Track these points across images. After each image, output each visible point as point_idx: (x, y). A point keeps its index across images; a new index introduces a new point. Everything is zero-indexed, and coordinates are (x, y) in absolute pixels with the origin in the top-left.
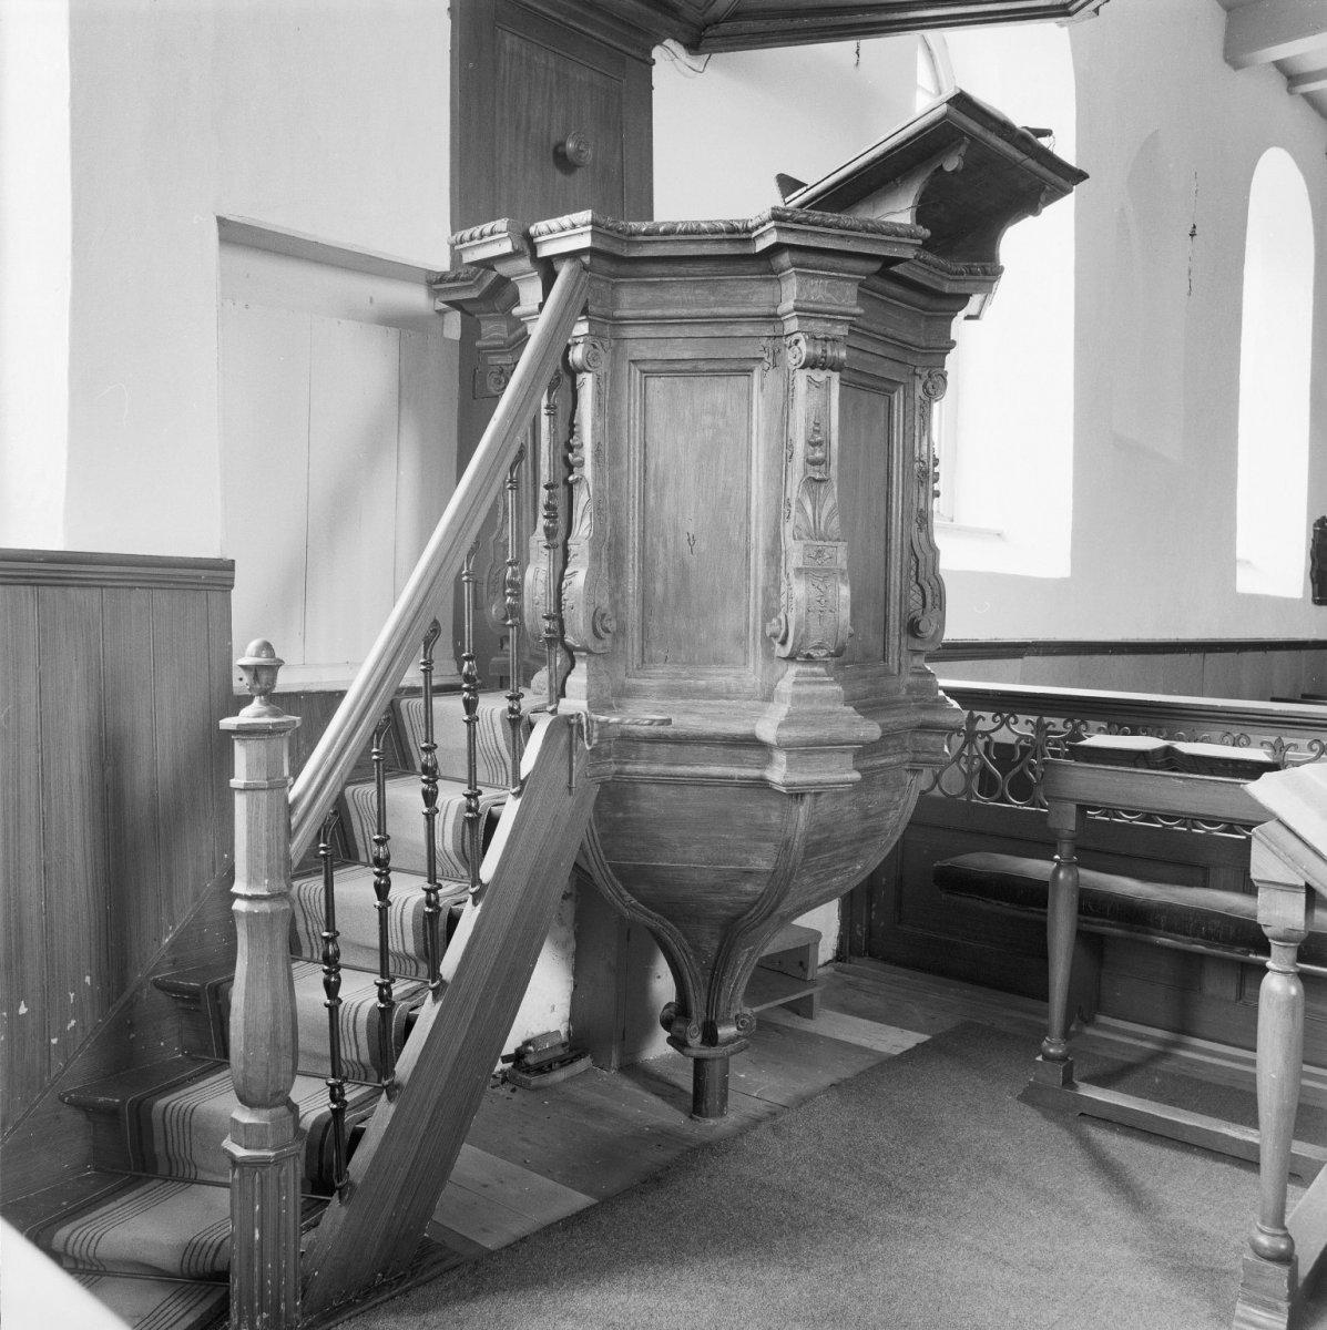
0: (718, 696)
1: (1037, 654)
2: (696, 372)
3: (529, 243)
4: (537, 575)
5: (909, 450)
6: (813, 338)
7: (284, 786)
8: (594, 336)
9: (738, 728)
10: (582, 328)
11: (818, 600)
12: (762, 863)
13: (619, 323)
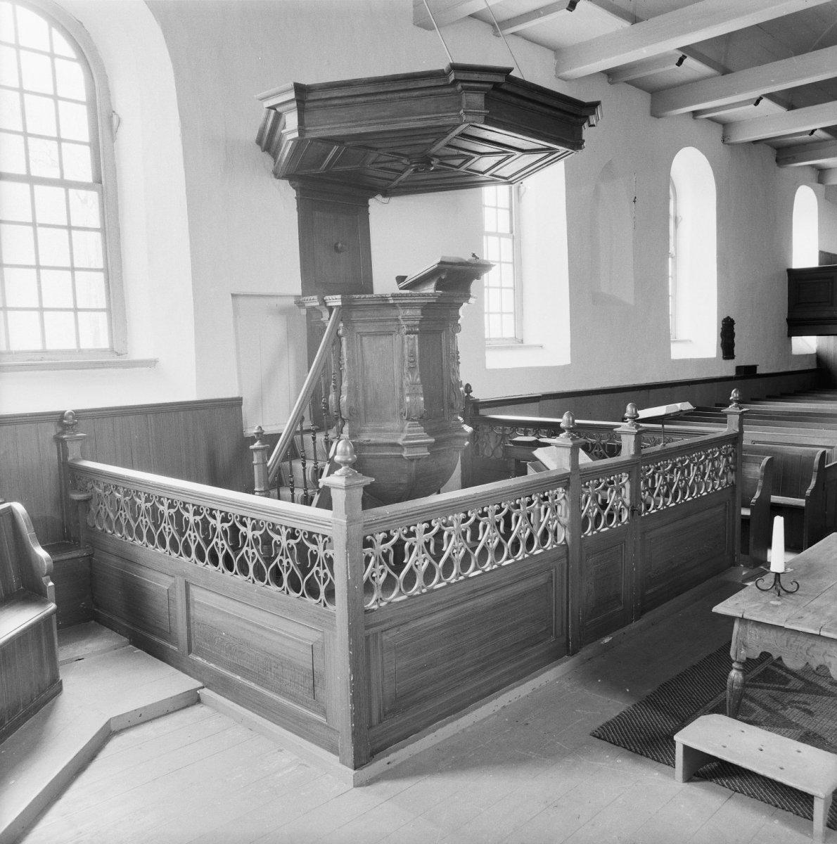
0: (388, 432)
1: (551, 399)
2: (376, 335)
3: (324, 302)
4: (332, 397)
5: (448, 349)
6: (408, 326)
7: (267, 462)
8: (346, 326)
9: (392, 441)
10: (341, 325)
11: (415, 401)
12: (404, 481)
13: (352, 322)
